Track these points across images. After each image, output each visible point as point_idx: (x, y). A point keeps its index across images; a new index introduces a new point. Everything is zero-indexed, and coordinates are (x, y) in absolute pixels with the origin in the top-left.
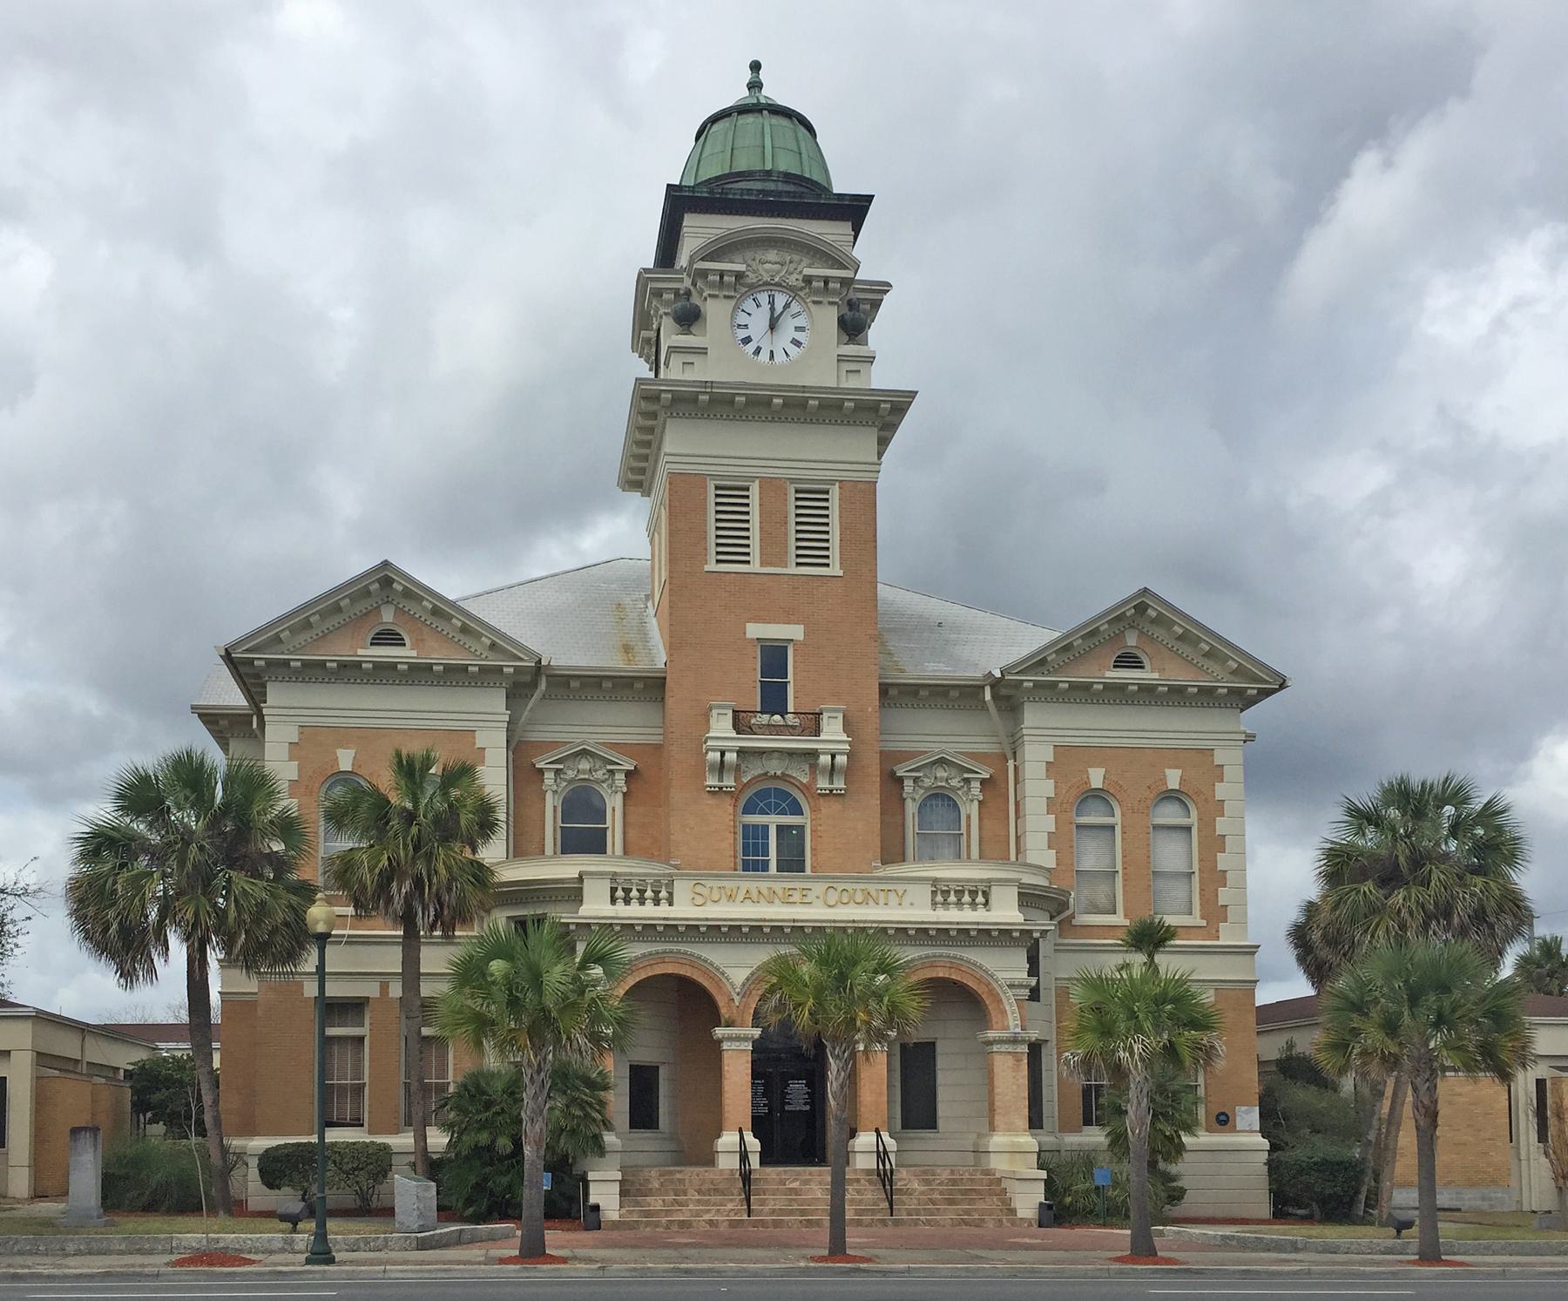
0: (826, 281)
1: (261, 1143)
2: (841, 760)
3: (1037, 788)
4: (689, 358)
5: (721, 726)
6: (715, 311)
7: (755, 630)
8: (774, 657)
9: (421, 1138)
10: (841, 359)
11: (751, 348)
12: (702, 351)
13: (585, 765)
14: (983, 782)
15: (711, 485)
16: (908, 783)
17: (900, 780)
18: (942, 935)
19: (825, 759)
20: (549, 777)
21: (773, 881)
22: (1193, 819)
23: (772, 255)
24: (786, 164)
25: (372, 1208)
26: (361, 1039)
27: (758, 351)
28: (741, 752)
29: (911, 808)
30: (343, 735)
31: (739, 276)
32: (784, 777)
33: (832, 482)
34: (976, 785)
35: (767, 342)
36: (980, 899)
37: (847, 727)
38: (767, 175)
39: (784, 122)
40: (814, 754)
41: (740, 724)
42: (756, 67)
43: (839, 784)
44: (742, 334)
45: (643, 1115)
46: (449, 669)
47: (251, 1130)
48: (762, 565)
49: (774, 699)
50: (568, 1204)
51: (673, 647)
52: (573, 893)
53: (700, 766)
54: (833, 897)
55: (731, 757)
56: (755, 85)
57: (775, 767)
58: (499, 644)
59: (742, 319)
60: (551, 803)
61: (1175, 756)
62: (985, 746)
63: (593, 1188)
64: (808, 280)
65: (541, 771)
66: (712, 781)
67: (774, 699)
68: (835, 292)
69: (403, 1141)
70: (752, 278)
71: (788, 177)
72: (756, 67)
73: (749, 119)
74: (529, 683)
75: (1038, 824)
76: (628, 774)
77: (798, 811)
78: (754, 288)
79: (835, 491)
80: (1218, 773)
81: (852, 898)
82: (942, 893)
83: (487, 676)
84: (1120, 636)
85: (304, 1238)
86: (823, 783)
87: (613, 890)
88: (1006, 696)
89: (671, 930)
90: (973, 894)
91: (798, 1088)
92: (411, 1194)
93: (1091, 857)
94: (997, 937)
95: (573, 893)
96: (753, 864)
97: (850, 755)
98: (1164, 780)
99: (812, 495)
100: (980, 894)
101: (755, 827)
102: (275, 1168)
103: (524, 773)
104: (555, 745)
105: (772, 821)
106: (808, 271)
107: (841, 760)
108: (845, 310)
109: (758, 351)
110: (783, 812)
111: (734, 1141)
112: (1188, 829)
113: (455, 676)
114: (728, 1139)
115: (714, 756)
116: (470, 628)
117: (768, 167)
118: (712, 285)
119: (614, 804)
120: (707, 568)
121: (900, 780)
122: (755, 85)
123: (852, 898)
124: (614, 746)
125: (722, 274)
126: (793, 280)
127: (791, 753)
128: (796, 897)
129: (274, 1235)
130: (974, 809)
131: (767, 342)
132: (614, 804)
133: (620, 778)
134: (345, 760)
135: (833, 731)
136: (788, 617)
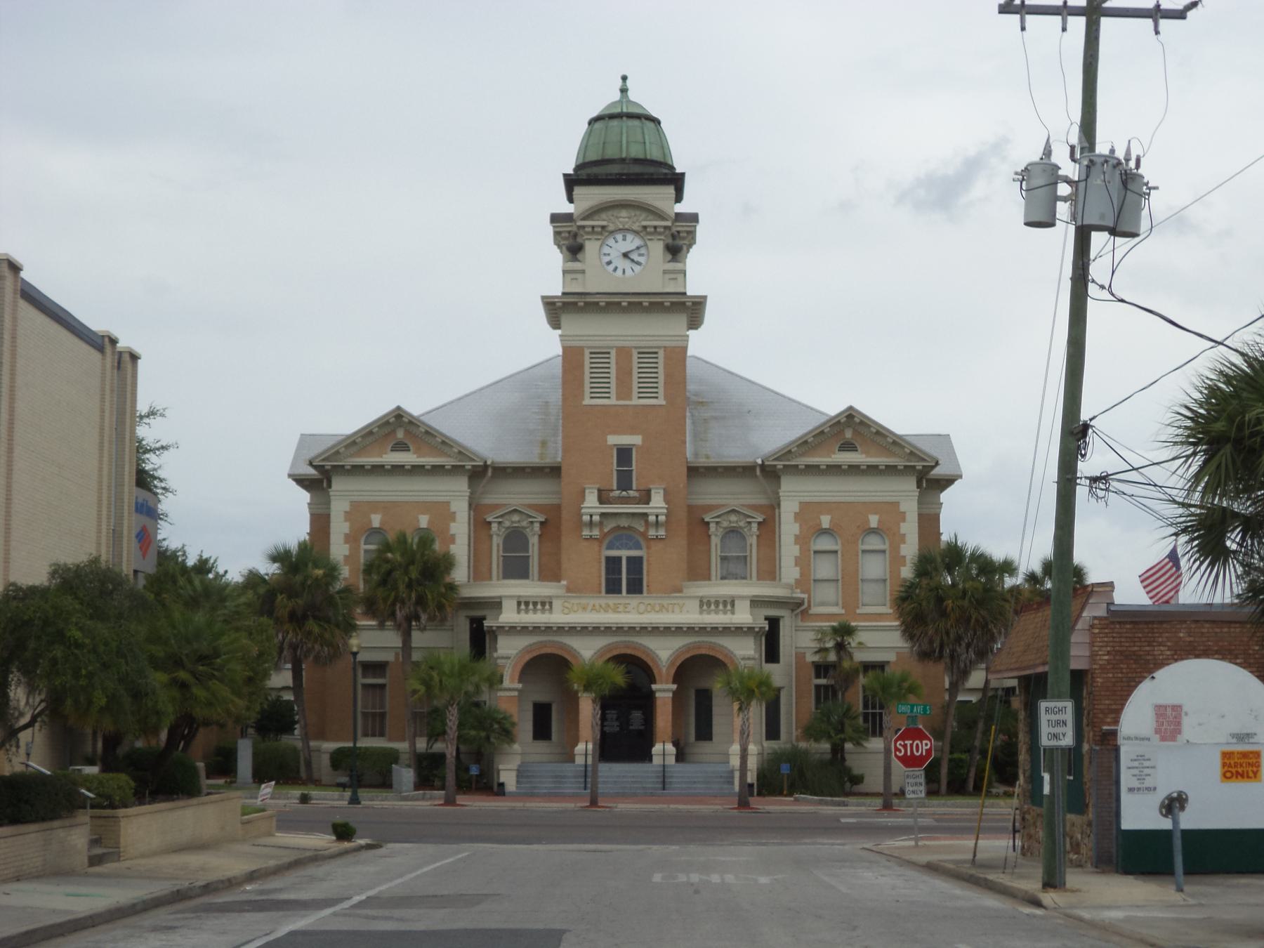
0: (655, 227)
1: (331, 746)
2: (662, 518)
3: (789, 528)
4: (574, 276)
5: (591, 501)
6: (591, 247)
7: (614, 440)
8: (624, 454)
9: (413, 744)
10: (665, 272)
11: (611, 268)
12: (583, 272)
13: (516, 518)
14: (759, 523)
15: (587, 352)
16: (712, 526)
17: (708, 524)
18: (702, 630)
19: (652, 518)
20: (494, 527)
21: (624, 599)
22: (886, 547)
23: (624, 213)
24: (636, 152)
25: (385, 783)
26: (382, 686)
27: (616, 269)
28: (603, 515)
29: (715, 541)
30: (374, 506)
31: (603, 227)
32: (630, 528)
33: (659, 347)
34: (755, 526)
35: (620, 263)
36: (729, 607)
37: (666, 500)
38: (623, 161)
39: (636, 123)
40: (646, 515)
41: (603, 498)
42: (624, 78)
43: (662, 532)
44: (607, 259)
45: (542, 730)
46: (434, 467)
47: (322, 736)
48: (618, 399)
49: (625, 481)
50: (488, 785)
51: (565, 451)
52: (496, 605)
53: (580, 525)
54: (642, 608)
55: (596, 518)
56: (624, 91)
57: (624, 523)
58: (463, 453)
59: (606, 250)
60: (497, 541)
61: (875, 507)
62: (760, 500)
63: (502, 773)
64: (645, 227)
65: (490, 523)
66: (586, 532)
67: (625, 481)
68: (660, 234)
69: (402, 746)
70: (611, 227)
71: (637, 161)
72: (624, 78)
73: (615, 123)
74: (481, 474)
75: (789, 550)
76: (542, 523)
77: (638, 547)
78: (612, 232)
79: (661, 354)
80: (902, 517)
81: (653, 608)
82: (706, 604)
83: (456, 470)
84: (841, 432)
85: (348, 794)
86: (652, 532)
87: (519, 604)
88: (769, 473)
89: (548, 629)
90: (725, 603)
91: (637, 716)
92: (405, 776)
93: (824, 569)
94: (738, 631)
95: (496, 605)
96: (613, 587)
97: (667, 516)
98: (868, 521)
99: (648, 353)
100: (729, 603)
101: (614, 558)
102: (338, 759)
103: (480, 525)
104: (497, 507)
105: (624, 553)
106: (645, 223)
107: (662, 518)
108: (670, 241)
109: (616, 269)
110: (630, 549)
111: (585, 748)
112: (836, 552)
113: (437, 470)
114: (580, 747)
115: (586, 518)
116: (445, 444)
117: (624, 155)
118: (588, 233)
119: (534, 541)
120: (585, 402)
121: (708, 524)
122: (624, 91)
123: (653, 608)
124: (530, 506)
125: (593, 227)
126: (635, 227)
127: (633, 514)
128: (621, 608)
129: (336, 794)
130: (754, 540)
131: (620, 263)
132: (534, 541)
133: (537, 526)
134: (376, 520)
135: (658, 502)
136: (632, 430)
